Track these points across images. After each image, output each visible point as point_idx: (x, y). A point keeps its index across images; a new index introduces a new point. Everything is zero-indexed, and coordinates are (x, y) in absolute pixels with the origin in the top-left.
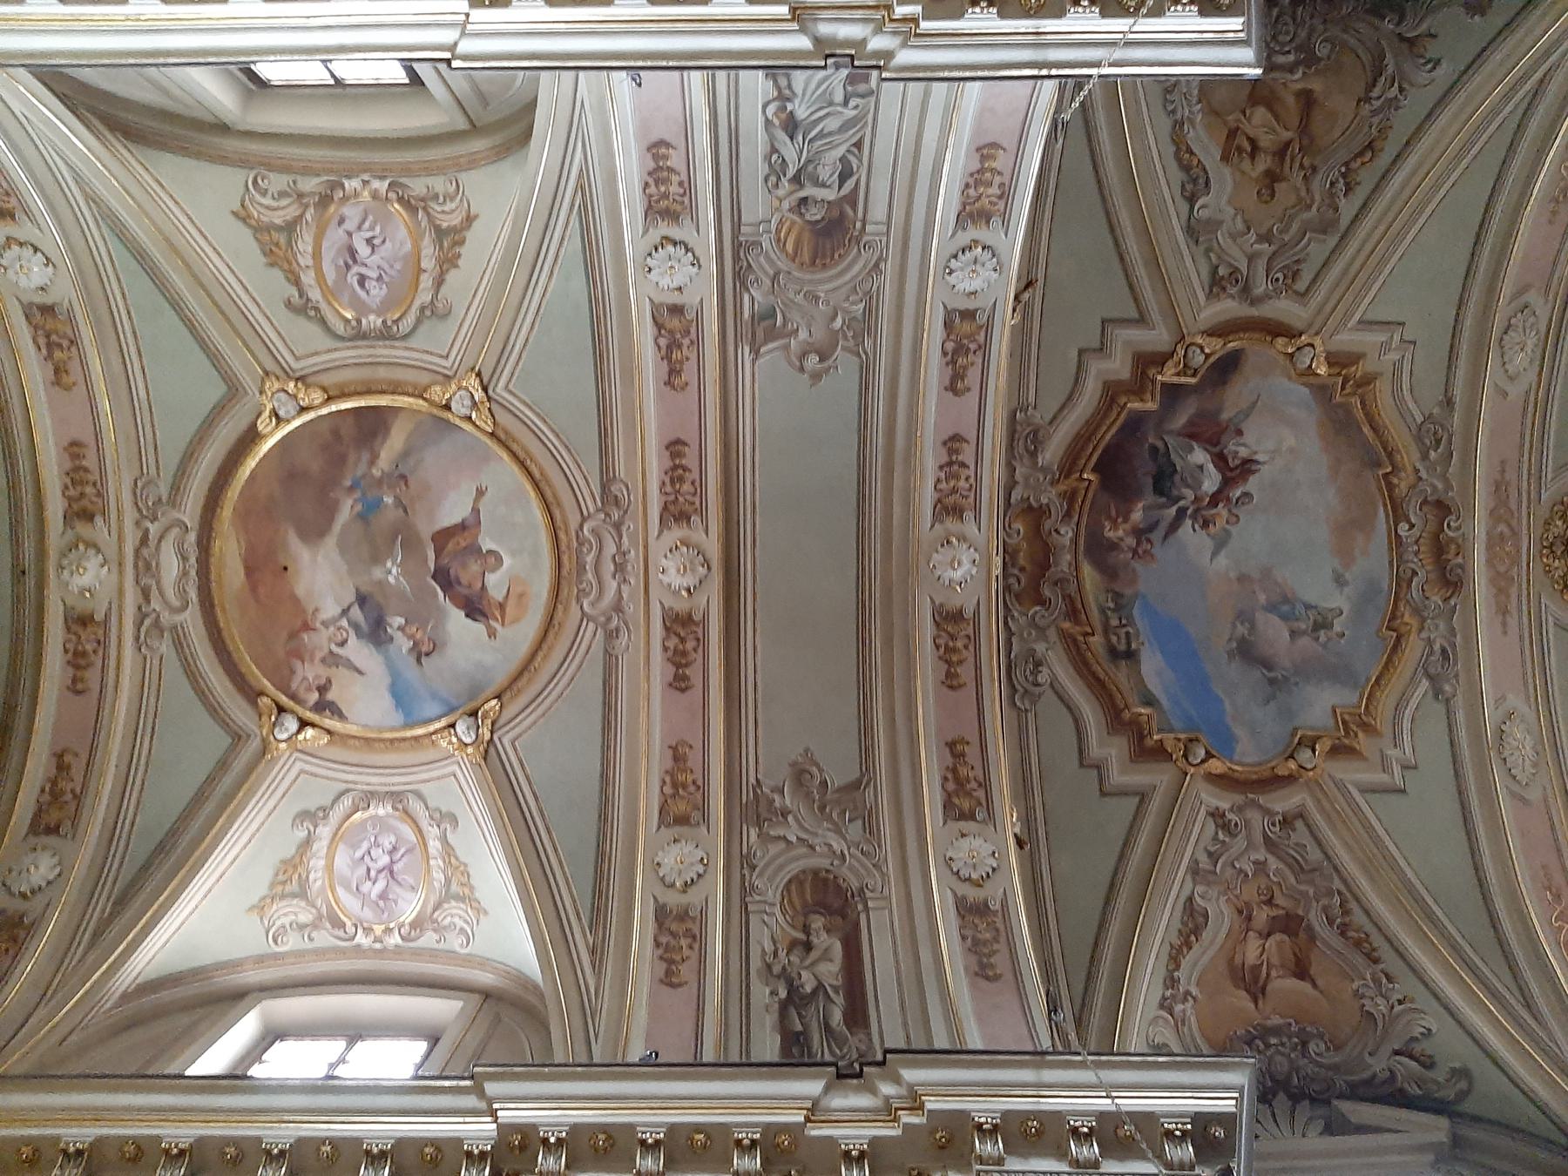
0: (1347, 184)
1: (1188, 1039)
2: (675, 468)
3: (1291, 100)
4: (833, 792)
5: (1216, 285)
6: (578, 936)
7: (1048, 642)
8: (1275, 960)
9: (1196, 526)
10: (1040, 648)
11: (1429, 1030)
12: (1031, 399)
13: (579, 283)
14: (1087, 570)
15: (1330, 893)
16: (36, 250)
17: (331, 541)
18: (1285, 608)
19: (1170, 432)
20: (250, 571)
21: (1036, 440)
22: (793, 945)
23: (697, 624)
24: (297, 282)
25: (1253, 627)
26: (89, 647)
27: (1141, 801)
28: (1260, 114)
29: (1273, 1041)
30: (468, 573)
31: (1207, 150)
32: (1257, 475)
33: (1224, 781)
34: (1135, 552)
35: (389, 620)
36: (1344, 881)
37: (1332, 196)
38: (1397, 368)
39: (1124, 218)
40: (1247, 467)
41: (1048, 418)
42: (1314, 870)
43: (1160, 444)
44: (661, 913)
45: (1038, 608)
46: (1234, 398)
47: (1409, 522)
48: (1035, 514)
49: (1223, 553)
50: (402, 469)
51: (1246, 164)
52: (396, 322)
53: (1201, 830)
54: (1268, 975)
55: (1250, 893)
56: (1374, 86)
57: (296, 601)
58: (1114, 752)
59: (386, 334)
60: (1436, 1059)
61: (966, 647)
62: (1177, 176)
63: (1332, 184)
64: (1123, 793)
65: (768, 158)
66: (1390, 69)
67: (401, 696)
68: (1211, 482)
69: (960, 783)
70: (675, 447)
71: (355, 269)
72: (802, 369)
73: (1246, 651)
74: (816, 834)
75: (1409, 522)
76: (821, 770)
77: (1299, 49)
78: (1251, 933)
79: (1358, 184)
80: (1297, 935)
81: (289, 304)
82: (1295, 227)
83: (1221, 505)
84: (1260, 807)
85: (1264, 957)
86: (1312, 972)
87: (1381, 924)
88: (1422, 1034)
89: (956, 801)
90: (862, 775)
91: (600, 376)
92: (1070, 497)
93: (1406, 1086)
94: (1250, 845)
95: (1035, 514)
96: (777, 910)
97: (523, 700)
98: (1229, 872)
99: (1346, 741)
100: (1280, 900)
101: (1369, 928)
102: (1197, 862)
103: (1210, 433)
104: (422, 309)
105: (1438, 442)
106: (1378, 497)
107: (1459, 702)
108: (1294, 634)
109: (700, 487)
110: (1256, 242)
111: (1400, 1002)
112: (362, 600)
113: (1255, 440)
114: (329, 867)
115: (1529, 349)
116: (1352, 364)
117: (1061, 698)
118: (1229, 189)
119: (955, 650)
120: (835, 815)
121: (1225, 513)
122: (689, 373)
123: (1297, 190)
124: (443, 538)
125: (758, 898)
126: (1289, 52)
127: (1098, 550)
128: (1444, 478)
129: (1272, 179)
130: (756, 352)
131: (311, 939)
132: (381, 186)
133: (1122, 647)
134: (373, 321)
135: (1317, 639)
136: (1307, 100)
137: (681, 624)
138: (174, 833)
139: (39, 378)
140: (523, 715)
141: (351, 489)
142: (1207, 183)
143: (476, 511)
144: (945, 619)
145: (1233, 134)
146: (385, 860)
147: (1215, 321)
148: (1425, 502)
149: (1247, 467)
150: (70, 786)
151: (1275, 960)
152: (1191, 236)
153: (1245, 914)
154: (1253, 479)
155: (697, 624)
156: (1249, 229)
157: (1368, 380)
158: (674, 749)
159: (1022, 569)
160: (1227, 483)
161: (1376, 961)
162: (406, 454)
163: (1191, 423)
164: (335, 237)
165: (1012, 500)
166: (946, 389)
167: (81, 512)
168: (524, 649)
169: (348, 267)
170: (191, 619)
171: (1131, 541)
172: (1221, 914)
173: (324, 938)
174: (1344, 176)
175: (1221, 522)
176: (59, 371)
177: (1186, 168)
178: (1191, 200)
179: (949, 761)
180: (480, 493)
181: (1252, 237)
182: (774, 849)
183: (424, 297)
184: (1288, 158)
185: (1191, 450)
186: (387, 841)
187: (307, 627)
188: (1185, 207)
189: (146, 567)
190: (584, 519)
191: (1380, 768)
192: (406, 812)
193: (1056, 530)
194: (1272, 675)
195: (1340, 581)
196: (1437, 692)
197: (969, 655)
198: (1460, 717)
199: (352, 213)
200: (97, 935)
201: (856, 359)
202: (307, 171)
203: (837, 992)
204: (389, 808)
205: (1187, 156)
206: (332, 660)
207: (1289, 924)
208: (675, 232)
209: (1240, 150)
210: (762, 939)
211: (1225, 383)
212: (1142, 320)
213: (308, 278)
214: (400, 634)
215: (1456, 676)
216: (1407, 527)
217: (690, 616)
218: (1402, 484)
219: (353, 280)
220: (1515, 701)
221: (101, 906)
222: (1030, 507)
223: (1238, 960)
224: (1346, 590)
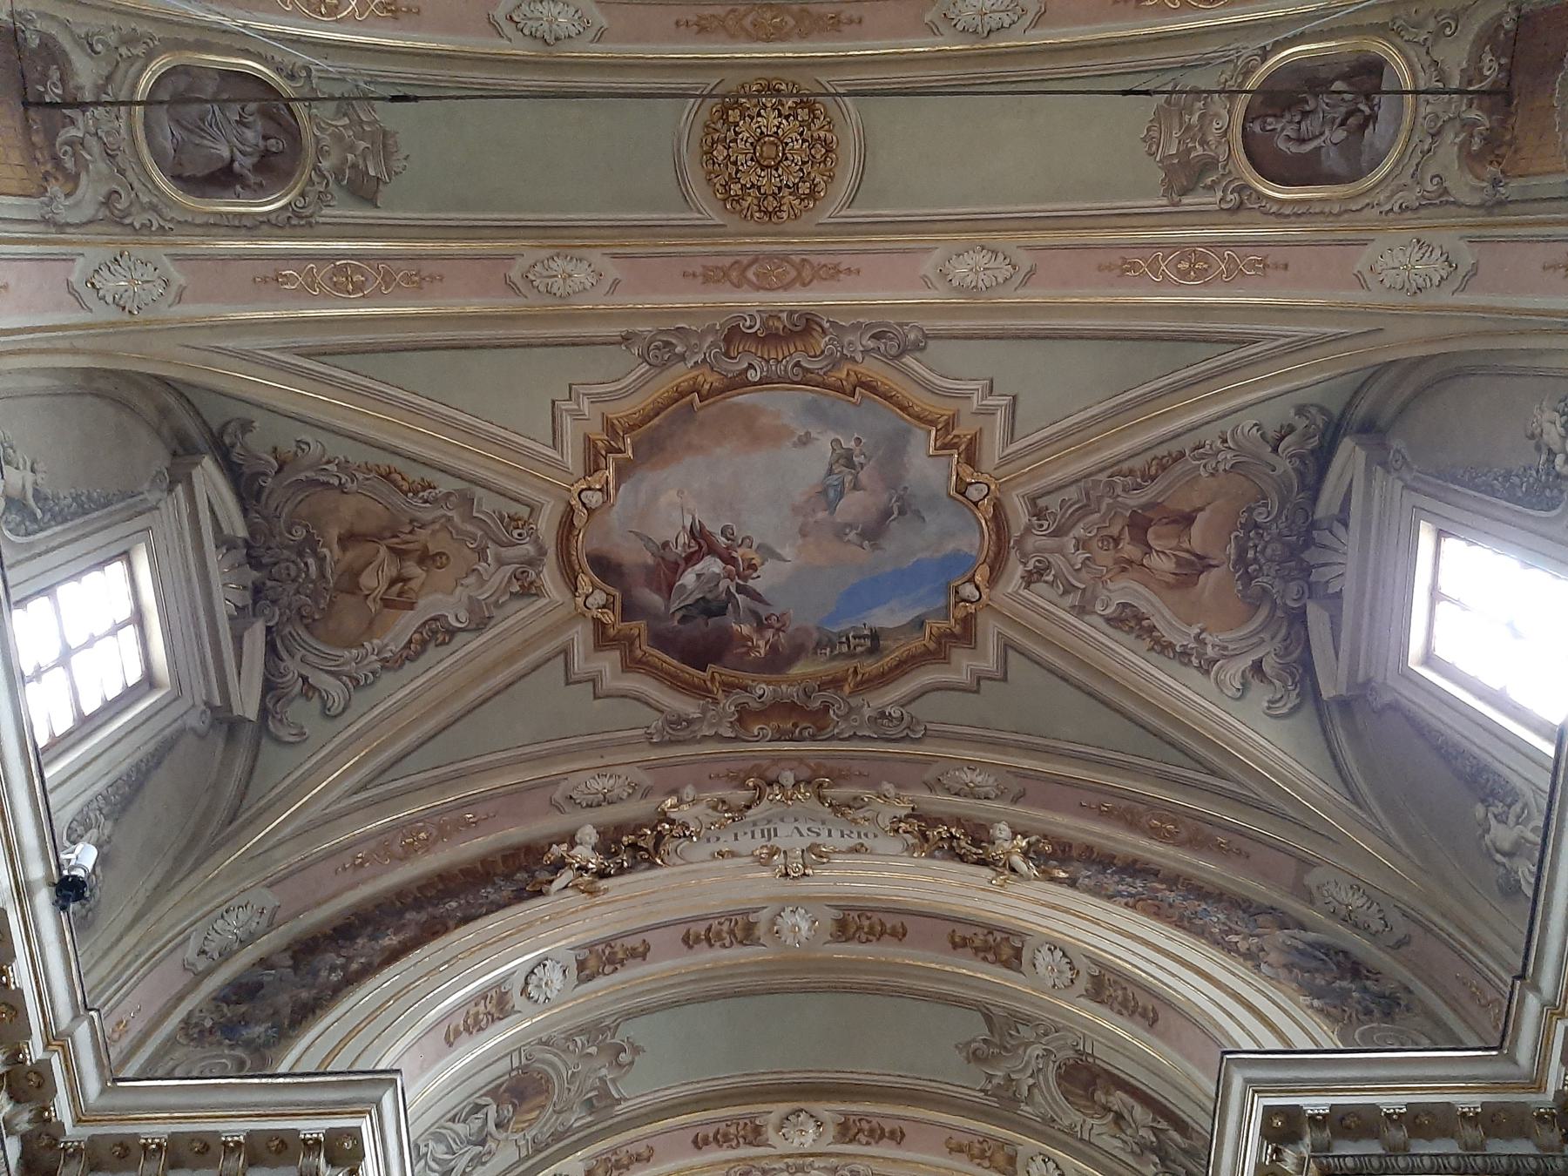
0: (424, 490)
1: (1244, 643)
3: (350, 555)
4: (993, 1036)
5: (529, 590)
7: (863, 706)
8: (1174, 543)
9: (755, 575)
10: (867, 712)
11: (1256, 425)
12: (641, 732)
14: (797, 670)
15: (1111, 485)
18: (832, 494)
19: (667, 607)
21: (678, 722)
23: (847, 1120)
25: (851, 526)
27: (1012, 647)
28: (367, 580)
29: (1251, 554)
31: (405, 625)
32: (705, 523)
33: (997, 566)
34: (778, 630)
36: (1101, 470)
37: (436, 500)
38: (596, 399)
39: (473, 695)
40: (698, 534)
41: (659, 714)
42: (1087, 495)
43: (678, 616)
45: (831, 712)
46: (632, 554)
47: (746, 370)
48: (744, 716)
49: (778, 551)
51: (414, 584)
53: (1041, 596)
54: (1187, 551)
55: (1105, 558)
56: (328, 483)
58: (965, 663)
60: (1285, 423)
61: (869, 918)
62: (432, 653)
63: (426, 502)
64: (1004, 661)
66: (311, 474)
68: (713, 565)
69: (987, 948)
70: (699, 1143)
72: (632, 1063)
73: (873, 533)
74: (1028, 1063)
75: (746, 370)
76: (974, 1040)
77: (301, 554)
78: (1145, 562)
79: (423, 480)
80: (1152, 520)
82: (469, 528)
83: (734, 554)
84: (1021, 536)
85: (1167, 551)
86: (1188, 510)
87: (1147, 446)
88: (1258, 430)
89: (1004, 957)
90: (980, 1011)
92: (728, 687)
93: (1309, 447)
94: (1060, 550)
95: (744, 716)
96: (1090, 1121)
98: (1084, 574)
99: (963, 447)
100: (1115, 531)
101: (1149, 456)
102: (1073, 607)
103: (666, 572)
105: (667, 344)
106: (719, 404)
107: (929, 325)
108: (856, 486)
109: (734, 1121)
110: (486, 562)
111: (1225, 441)
113: (671, 528)
115: (569, 267)
116: (595, 446)
117: (914, 700)
118: (440, 596)
119: (871, 927)
120: (1013, 1043)
121: (740, 551)
122: (641, 1148)
123: (434, 533)
125: (1078, 1128)
126: (306, 564)
127: (776, 662)
128: (702, 336)
129: (426, 558)
130: (618, 1102)
133: (868, 643)
135: (862, 466)
136: (347, 539)
137: (846, 1131)
142: (435, 619)
144: (843, 933)
145: (387, 603)
147: (561, 584)
148: (727, 354)
149: (698, 534)
151: (1174, 543)
152: (486, 625)
153: (1125, 566)
154: (709, 527)
155: (847, 1120)
156: (474, 570)
157: (609, 426)
158: (951, 1150)
159: (795, 725)
160: (712, 550)
161: (1182, 454)
163: (658, 590)
165: (733, 735)
166: (644, 959)
167: (746, 933)
171: (769, 634)
172: (1123, 591)
174: (416, 493)
175: (751, 554)
177: (424, 644)
178: (452, 632)
179: (969, 950)
181: (482, 566)
182: (1038, 1098)
184: (403, 547)
185: (683, 586)
188: (460, 638)
191: (992, 417)
193: (760, 698)
194: (896, 513)
195: (805, 441)
196: (918, 347)
197: (876, 917)
198: (942, 324)
201: (621, 1026)
204: (991, 780)
205: (412, 646)
207: (1139, 525)
209: (400, 594)
211: (620, 565)
212: (566, 652)
215: (901, 325)
216: (751, 372)
218: (710, 379)
220: (928, 266)
222: (739, 720)
223: (1171, 579)
224: (814, 435)
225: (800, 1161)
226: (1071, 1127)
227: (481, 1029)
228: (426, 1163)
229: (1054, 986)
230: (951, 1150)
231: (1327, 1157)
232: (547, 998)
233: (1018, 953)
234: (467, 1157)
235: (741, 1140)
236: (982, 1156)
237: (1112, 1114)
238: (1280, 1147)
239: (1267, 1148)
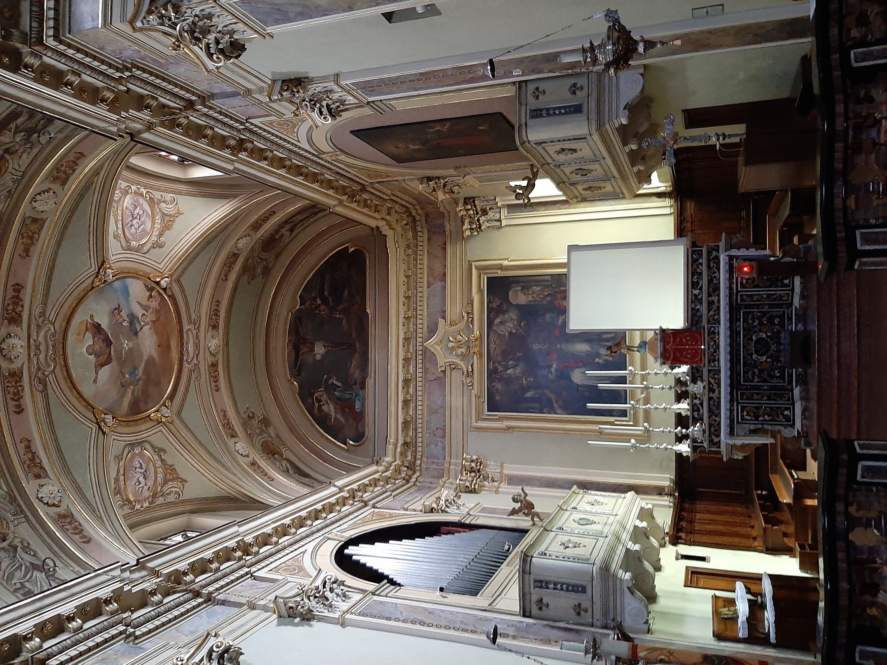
2: (18, 400)
6: (100, 181)
13: (79, 480)
16: (242, 455)
17: (145, 358)
20: (169, 346)
22: (11, 154)
23: (6, 318)
24: (162, 460)
26: (213, 317)
30: (100, 345)
35: (128, 324)
44: (64, 183)
50: (123, 389)
52: (130, 452)
57: (156, 333)
59: (132, 445)
65: (35, 552)
67: (126, 292)
71: (143, 471)
81: (165, 451)
91: (56, 440)
96: (10, 169)
97: (84, 285)
104: (122, 459)
112: (136, 333)
114: (153, 223)
122: (21, 447)
124: (108, 361)
125: (15, 177)
131: (161, 195)
132: (138, 507)
134: (137, 451)
138: (203, 248)
139: (229, 413)
140: (83, 280)
141: (139, 380)
143: (96, 373)
146: (134, 222)
150: (24, 240)
158: (27, 255)
162: (123, 396)
164: (150, 483)
168: (80, 310)
169: (146, 471)
170: (186, 327)
173: (157, 195)
176: (225, 416)
180: (95, 381)
183: (122, 464)
186: (133, 230)
187: (154, 322)
189: (197, 346)
190: (53, 371)
192: (127, 242)
199: (146, 494)
200: (237, 219)
202: (161, 505)
203: (11, 128)
206: (146, 308)
208: (58, 510)
210: (25, 159)
213: (159, 463)
214: (125, 319)
217: (10, 323)
219: (144, 466)
221: (231, 227)
225: (33, 348)
226: (14, 182)
227: (80, 524)
228: (27, 581)
229: (56, 203)
230: (27, 255)
231: (31, 38)
232: (58, 492)
233: (35, 220)
234: (25, 556)
235: (18, 384)
236: (31, 238)
237: (6, 155)
238: (23, 64)
239: (23, 72)
